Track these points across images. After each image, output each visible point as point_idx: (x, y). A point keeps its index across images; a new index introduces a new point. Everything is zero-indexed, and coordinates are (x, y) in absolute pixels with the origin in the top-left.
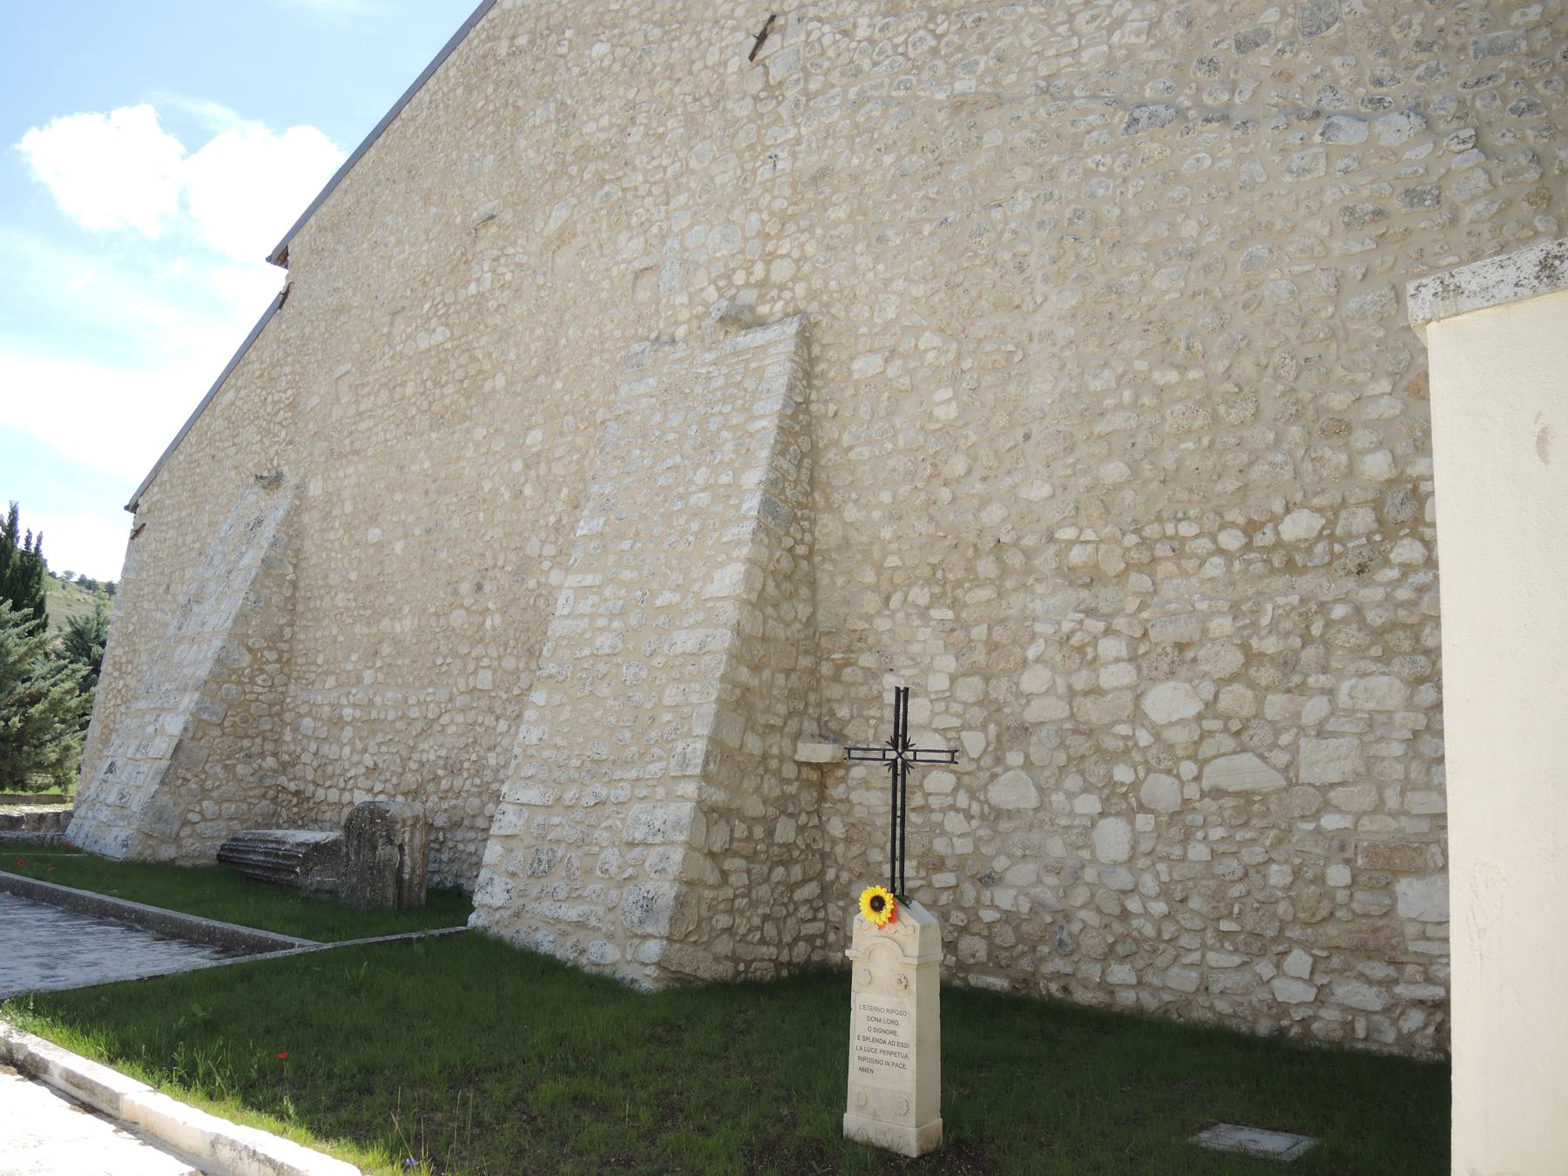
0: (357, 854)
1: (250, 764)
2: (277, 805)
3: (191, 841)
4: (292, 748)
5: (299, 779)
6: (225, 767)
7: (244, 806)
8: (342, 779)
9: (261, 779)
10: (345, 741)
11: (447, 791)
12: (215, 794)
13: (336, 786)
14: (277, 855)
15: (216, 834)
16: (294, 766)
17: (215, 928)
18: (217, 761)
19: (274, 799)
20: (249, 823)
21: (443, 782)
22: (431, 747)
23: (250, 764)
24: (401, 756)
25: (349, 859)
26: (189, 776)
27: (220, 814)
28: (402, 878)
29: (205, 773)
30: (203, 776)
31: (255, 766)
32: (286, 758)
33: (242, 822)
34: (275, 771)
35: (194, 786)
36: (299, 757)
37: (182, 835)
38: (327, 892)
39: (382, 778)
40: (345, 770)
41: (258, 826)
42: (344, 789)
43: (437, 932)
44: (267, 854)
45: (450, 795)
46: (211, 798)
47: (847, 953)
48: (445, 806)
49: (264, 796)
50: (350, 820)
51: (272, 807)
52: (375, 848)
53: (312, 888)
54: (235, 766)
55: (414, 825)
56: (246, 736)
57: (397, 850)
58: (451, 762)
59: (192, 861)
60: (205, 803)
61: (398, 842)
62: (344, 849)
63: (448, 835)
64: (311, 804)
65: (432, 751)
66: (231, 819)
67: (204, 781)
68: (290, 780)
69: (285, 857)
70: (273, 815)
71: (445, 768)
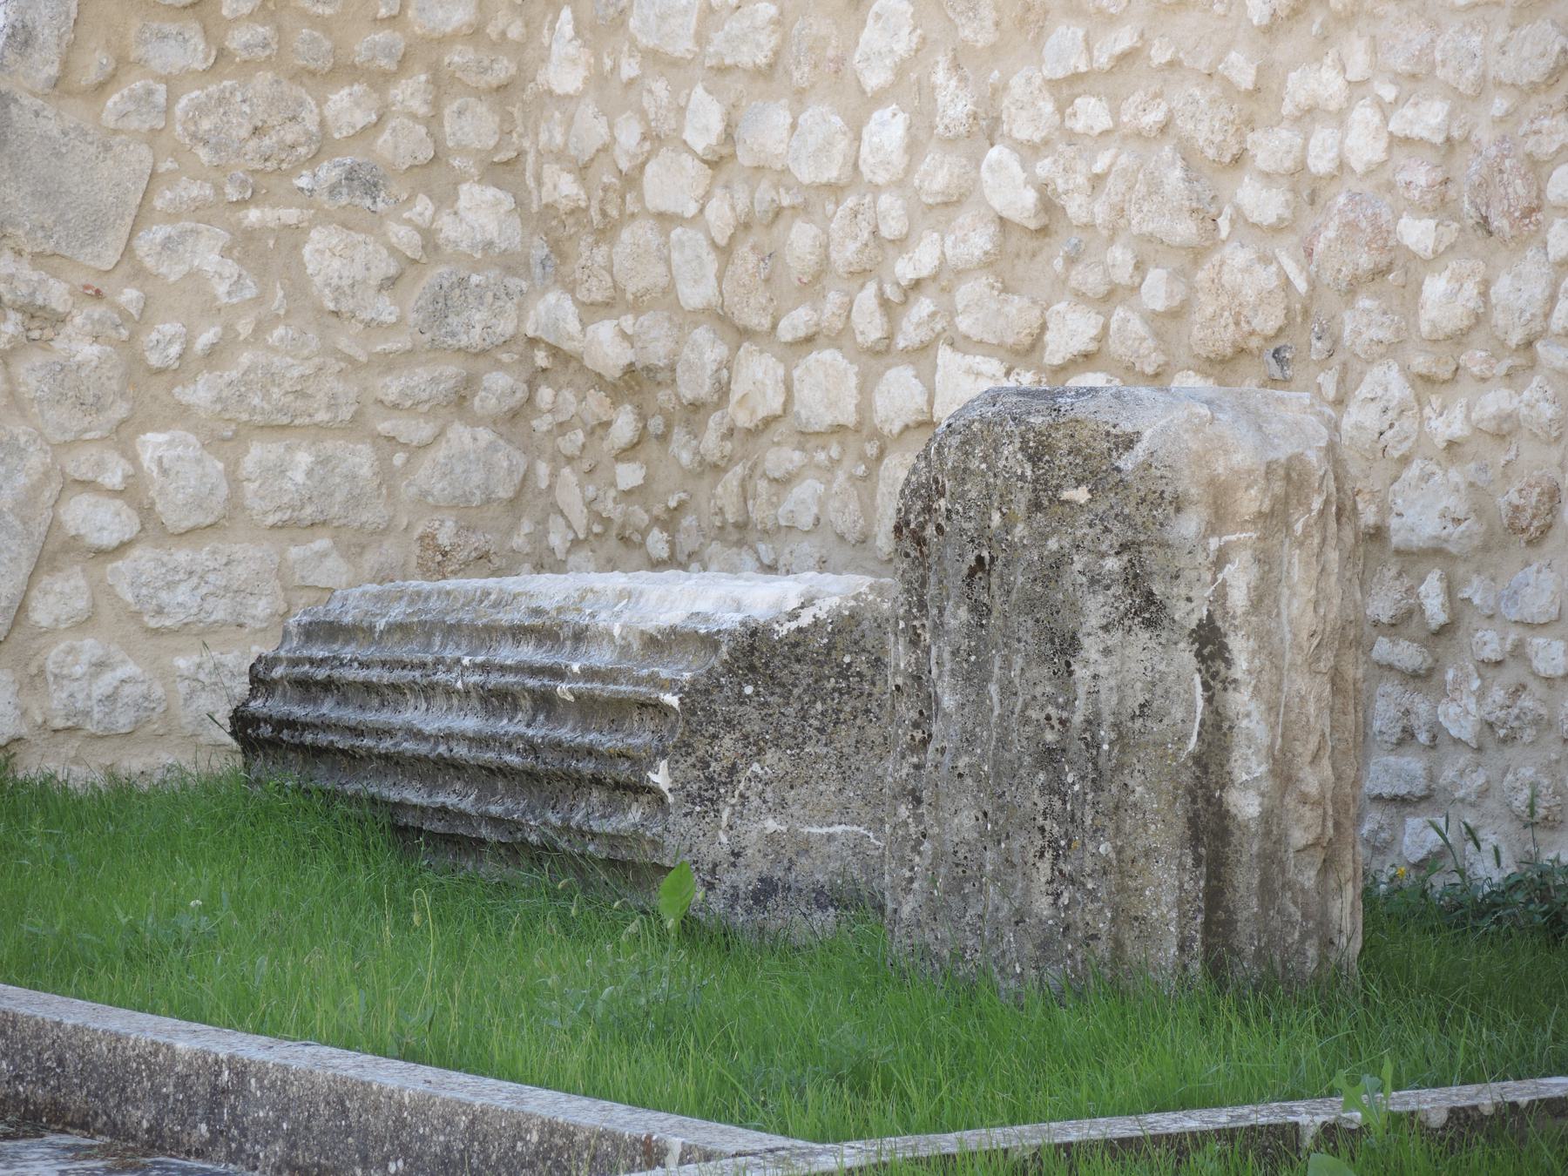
0: (973, 676)
1: (373, 224)
2: (530, 449)
3: (90, 647)
4: (591, 128)
5: (637, 306)
6: (245, 244)
7: (361, 459)
8: (867, 298)
9: (441, 307)
10: (875, 79)
11: (1459, 339)
12: (199, 393)
13: (840, 337)
14: (545, 702)
15: (220, 611)
16: (606, 232)
17: (241, 1071)
18: (200, 211)
19: (516, 417)
20: (389, 551)
21: (1435, 287)
22: (1357, 88)
23: (373, 224)
24: (1188, 155)
25: (931, 702)
26: (57, 294)
27: (235, 504)
28: (1222, 814)
29: (139, 274)
30: (129, 296)
31: (402, 235)
32: (564, 187)
33: (354, 544)
34: (512, 264)
35: (88, 351)
36: (631, 180)
37: (42, 613)
38: (823, 898)
39: (1090, 278)
40: (884, 246)
41: (438, 560)
42: (882, 352)
43: (1433, 1104)
44: (496, 700)
45: (1475, 359)
46: (184, 413)
47: (1243, 89)
48: (1448, 424)
49: (460, 400)
50: (923, 493)
51: (507, 459)
52: (1069, 645)
53: (745, 878)
54: (294, 236)
55: (1274, 518)
56: (343, 71)
57: (1185, 656)
58: (1471, 168)
59: (103, 756)
60: (153, 445)
61: (1189, 612)
62: (899, 656)
63: (1475, 591)
64: (711, 442)
65: (1364, 115)
66: (293, 527)
67: (139, 321)
68: (591, 311)
69: (588, 708)
70: (514, 504)
71: (1440, 205)
